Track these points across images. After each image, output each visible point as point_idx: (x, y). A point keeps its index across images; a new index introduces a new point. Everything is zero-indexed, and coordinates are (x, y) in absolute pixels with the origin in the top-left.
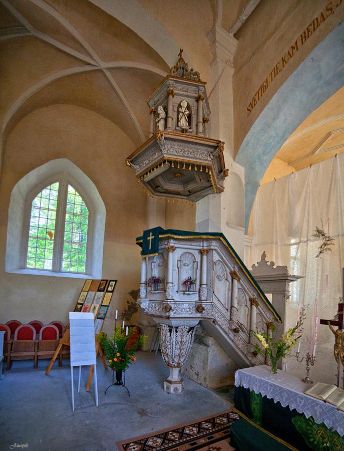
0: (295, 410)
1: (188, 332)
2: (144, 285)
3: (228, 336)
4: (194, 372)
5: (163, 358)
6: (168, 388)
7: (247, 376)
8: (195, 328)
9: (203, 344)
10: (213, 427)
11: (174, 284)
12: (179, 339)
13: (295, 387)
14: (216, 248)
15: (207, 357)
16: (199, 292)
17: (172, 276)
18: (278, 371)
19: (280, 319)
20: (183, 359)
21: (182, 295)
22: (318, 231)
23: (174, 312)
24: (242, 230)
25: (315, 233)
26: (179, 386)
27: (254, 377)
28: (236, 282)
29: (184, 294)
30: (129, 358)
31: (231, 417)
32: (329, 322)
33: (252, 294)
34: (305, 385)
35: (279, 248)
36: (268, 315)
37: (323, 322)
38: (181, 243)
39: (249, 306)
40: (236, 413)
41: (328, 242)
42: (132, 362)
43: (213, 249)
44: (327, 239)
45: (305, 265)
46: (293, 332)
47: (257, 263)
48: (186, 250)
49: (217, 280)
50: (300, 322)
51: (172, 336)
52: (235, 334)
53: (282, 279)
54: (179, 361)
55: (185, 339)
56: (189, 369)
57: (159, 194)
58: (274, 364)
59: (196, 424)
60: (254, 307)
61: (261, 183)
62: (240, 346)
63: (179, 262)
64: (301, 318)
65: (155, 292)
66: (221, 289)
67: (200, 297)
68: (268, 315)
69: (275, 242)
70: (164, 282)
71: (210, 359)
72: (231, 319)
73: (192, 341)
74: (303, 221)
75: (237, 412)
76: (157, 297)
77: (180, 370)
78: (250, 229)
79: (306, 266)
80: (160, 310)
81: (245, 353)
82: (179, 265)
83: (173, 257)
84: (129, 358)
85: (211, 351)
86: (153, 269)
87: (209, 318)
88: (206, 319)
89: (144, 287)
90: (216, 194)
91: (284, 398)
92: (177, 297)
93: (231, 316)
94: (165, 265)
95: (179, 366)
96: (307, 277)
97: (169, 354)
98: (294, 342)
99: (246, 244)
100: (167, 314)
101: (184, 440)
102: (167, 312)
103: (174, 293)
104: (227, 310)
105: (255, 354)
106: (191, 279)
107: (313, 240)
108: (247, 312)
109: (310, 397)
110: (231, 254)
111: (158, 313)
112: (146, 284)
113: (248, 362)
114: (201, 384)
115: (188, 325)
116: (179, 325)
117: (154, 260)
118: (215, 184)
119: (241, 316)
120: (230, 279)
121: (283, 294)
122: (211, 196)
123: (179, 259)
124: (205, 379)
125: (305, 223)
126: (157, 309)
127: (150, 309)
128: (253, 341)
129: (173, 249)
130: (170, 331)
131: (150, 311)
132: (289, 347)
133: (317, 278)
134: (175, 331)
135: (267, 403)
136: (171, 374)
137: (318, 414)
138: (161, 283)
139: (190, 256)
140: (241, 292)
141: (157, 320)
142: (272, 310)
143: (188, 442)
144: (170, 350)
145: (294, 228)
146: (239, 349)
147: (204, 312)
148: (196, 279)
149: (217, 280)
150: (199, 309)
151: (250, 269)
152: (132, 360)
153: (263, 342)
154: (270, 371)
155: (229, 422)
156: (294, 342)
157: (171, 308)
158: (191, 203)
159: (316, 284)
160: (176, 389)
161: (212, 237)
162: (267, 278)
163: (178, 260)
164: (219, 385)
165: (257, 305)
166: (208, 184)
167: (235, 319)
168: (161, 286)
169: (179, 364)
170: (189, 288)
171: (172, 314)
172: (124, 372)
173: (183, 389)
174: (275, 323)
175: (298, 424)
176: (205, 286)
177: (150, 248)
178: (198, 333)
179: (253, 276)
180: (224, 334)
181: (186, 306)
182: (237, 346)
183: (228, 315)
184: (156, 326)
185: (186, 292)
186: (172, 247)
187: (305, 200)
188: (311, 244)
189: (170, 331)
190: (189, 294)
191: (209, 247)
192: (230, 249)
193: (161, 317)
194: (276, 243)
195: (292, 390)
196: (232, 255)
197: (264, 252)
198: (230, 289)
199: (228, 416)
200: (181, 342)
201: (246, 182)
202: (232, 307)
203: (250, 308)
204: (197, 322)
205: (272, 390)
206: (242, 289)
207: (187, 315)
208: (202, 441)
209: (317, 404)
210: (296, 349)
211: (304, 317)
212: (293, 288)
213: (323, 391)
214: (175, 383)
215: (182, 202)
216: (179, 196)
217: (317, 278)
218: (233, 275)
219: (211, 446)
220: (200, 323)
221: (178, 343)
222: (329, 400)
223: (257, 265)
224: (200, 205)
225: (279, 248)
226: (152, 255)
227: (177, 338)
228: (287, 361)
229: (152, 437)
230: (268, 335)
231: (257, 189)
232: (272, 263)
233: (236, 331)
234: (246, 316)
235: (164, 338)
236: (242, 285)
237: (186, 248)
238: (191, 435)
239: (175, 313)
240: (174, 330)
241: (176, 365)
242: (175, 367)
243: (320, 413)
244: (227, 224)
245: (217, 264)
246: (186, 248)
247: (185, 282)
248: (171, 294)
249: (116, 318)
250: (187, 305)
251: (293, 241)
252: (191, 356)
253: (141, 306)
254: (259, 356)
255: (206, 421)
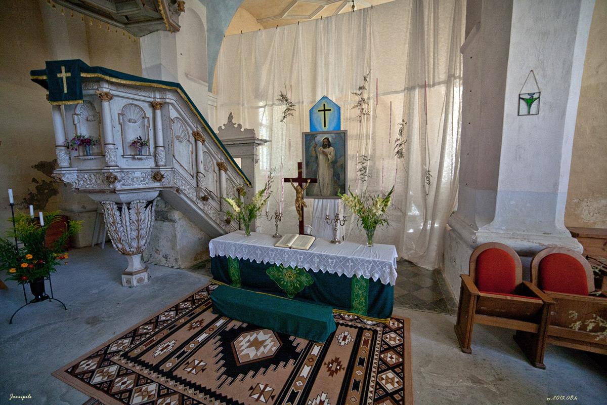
0: (268, 263)
1: (146, 207)
2: (63, 148)
3: (197, 205)
4: (161, 256)
5: (114, 246)
6: (129, 282)
7: (222, 244)
8: (155, 201)
9: (168, 220)
10: (193, 304)
11: (116, 146)
12: (134, 217)
13: (268, 243)
14: (172, 101)
15: (175, 234)
16: (155, 156)
17: (111, 134)
18: (251, 233)
19: (250, 184)
20: (144, 241)
21: (130, 161)
22: (282, 96)
23: (122, 182)
24: (205, 85)
25: (280, 97)
26: (144, 275)
27: (229, 243)
28: (200, 144)
29: (134, 159)
30: (55, 258)
31: (210, 289)
32: (291, 180)
33: (220, 158)
34: (275, 240)
35: (246, 110)
36: (238, 181)
37: (287, 180)
38: (122, 90)
39: (217, 172)
40: (215, 284)
41: (291, 108)
42: (62, 262)
43: (169, 103)
44: (290, 105)
45: (271, 128)
46: (262, 192)
47: (224, 125)
48: (131, 101)
49: (176, 142)
50: (269, 185)
51: (123, 216)
52: (204, 202)
53: (250, 142)
54: (138, 246)
55: (142, 217)
56: (154, 253)
57: (70, 6)
58: (247, 227)
59: (173, 307)
60: (223, 172)
61: (227, 32)
62: (211, 216)
63: (121, 118)
64: (269, 181)
65: (86, 157)
66: (183, 151)
67: (156, 162)
68: (238, 181)
69: (242, 103)
70: (100, 144)
71: (179, 236)
72: (198, 186)
73: (153, 218)
74: (269, 84)
75: (216, 283)
76: (92, 164)
77: (142, 256)
78: (214, 85)
79: (272, 131)
80: (99, 181)
81: (218, 223)
82: (121, 121)
83: (111, 110)
84: (55, 258)
85: (179, 227)
86: (78, 125)
87: (172, 187)
88: (166, 189)
89: (63, 152)
90: (170, 33)
91: (259, 255)
92: (123, 163)
93: (197, 183)
94: (98, 119)
95: (139, 251)
96: (273, 141)
97: (123, 238)
98: (264, 203)
99: (210, 103)
100: (111, 186)
101: (161, 327)
102: (110, 183)
103: (117, 157)
104: (193, 176)
105: (228, 222)
106: (141, 139)
107: (278, 105)
108: (215, 178)
109: (279, 248)
110: (192, 110)
111: (96, 187)
112: (68, 148)
113: (222, 232)
114: (172, 267)
115: (145, 198)
116: (131, 200)
117: (78, 112)
118: (167, 18)
119: (209, 183)
120: (192, 140)
121: (252, 159)
122: (162, 33)
123: (120, 112)
124: (176, 260)
125: (271, 87)
126: (93, 181)
127: (82, 182)
128: (225, 209)
129: (109, 97)
130: (120, 209)
131: (82, 185)
132: (260, 208)
133: (282, 137)
134: (126, 208)
135: (244, 264)
136: (130, 263)
137: (286, 260)
138: (94, 145)
139: (138, 110)
140: (208, 157)
141: (95, 197)
142: (241, 175)
143: (166, 328)
144: (123, 234)
145: (260, 91)
146: (211, 218)
147: (163, 180)
148: (148, 139)
149: (176, 142)
150: (157, 177)
151: (216, 132)
152: (61, 258)
153: (234, 207)
154: (244, 234)
155: (209, 294)
156: (264, 203)
157: (116, 178)
158: (133, 37)
159: (281, 148)
160: (140, 280)
161: (167, 87)
162: (234, 141)
163: (119, 114)
164: (194, 263)
165: (226, 170)
166: (155, 15)
167: (203, 185)
168: (95, 149)
169: (139, 248)
170: (140, 151)
171: (118, 186)
172: (49, 278)
173: (149, 278)
174: (246, 189)
175: (271, 274)
176: (161, 148)
177: (66, 91)
178: (159, 209)
179: (220, 139)
180: (191, 204)
181: (138, 174)
182: (207, 215)
183: (193, 182)
184: (96, 211)
185: (136, 157)
186: (107, 94)
187: (271, 63)
188: (276, 108)
189: (120, 209)
190: (141, 159)
191: (162, 100)
192: (190, 104)
193: (102, 192)
194: (243, 105)
195: (265, 246)
196: (194, 113)
197: (231, 113)
198: (194, 153)
199: (207, 289)
200: (137, 221)
201: (208, 27)
202: (198, 172)
203: (218, 174)
204: (157, 194)
205: (247, 251)
206: (208, 153)
207: (142, 186)
208: (182, 321)
209: (285, 252)
210: (266, 207)
211: (272, 180)
212: (262, 152)
213: (289, 240)
214: (138, 272)
215: (115, 31)
216: (110, 21)
217: (282, 137)
218: (196, 135)
219: (193, 321)
220: (160, 195)
221: (133, 222)
222: (294, 246)
223: (223, 127)
224: (146, 42)
225: (246, 110)
226: (71, 103)
227: (132, 216)
228: (260, 222)
229: (115, 342)
230: (239, 199)
231: (221, 40)
232: (240, 126)
233: (205, 199)
234: (215, 182)
235: (111, 220)
236: (208, 149)
237: (131, 99)
238: (168, 320)
239: (123, 185)
240: (125, 207)
241: (135, 250)
242: (133, 254)
243: (287, 259)
244: (187, 75)
245: (176, 121)
246: (131, 99)
247: (133, 143)
248: (113, 158)
249: (12, 201)
250: (140, 173)
251: (261, 104)
252: (154, 238)
253: (63, 179)
254: (232, 223)
255: (184, 301)
